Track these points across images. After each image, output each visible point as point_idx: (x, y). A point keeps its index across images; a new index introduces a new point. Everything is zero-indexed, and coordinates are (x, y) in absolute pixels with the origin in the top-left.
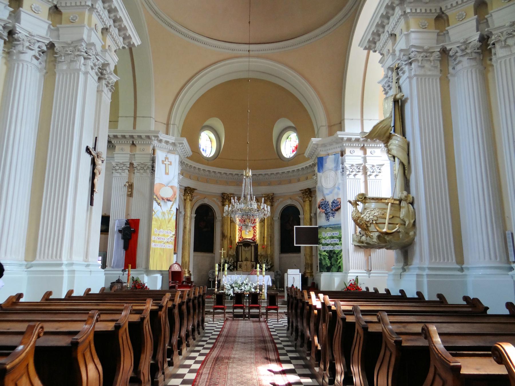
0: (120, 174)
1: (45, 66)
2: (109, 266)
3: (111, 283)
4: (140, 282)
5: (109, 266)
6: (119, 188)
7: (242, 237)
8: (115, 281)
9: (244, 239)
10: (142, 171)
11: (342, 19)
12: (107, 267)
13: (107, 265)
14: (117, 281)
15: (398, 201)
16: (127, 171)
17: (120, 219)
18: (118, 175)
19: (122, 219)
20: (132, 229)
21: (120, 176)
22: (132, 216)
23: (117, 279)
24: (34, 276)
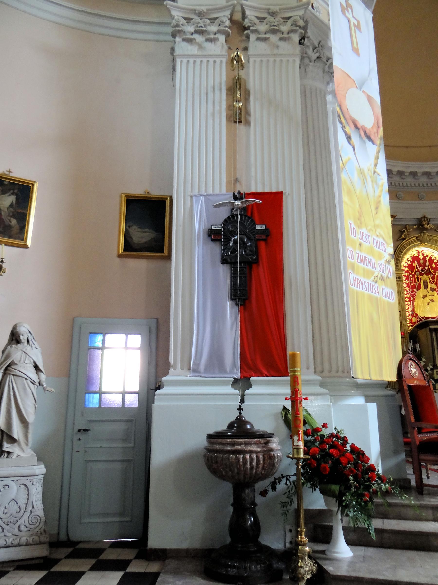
0: (200, 47)
1: (27, 503)
2: (179, 366)
3: (210, 437)
4: (326, 432)
5: (179, 366)
6: (197, 92)
7: (417, 315)
8: (222, 427)
9: (421, 320)
10: (274, 38)
11: (314, 135)
12: (171, 370)
13: (171, 361)
14: (231, 426)
15: (99, 390)
16: (222, 38)
17: (210, 192)
18: (192, 49)
19: (217, 191)
20: (258, 227)
21: (200, 53)
22: (253, 183)
23: (233, 418)
24: (332, 408)
